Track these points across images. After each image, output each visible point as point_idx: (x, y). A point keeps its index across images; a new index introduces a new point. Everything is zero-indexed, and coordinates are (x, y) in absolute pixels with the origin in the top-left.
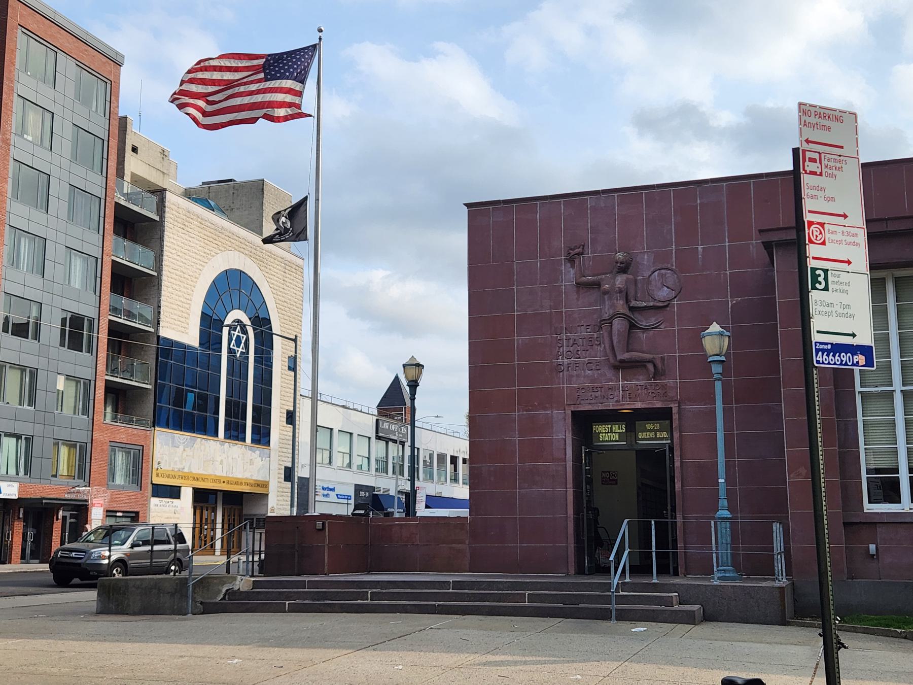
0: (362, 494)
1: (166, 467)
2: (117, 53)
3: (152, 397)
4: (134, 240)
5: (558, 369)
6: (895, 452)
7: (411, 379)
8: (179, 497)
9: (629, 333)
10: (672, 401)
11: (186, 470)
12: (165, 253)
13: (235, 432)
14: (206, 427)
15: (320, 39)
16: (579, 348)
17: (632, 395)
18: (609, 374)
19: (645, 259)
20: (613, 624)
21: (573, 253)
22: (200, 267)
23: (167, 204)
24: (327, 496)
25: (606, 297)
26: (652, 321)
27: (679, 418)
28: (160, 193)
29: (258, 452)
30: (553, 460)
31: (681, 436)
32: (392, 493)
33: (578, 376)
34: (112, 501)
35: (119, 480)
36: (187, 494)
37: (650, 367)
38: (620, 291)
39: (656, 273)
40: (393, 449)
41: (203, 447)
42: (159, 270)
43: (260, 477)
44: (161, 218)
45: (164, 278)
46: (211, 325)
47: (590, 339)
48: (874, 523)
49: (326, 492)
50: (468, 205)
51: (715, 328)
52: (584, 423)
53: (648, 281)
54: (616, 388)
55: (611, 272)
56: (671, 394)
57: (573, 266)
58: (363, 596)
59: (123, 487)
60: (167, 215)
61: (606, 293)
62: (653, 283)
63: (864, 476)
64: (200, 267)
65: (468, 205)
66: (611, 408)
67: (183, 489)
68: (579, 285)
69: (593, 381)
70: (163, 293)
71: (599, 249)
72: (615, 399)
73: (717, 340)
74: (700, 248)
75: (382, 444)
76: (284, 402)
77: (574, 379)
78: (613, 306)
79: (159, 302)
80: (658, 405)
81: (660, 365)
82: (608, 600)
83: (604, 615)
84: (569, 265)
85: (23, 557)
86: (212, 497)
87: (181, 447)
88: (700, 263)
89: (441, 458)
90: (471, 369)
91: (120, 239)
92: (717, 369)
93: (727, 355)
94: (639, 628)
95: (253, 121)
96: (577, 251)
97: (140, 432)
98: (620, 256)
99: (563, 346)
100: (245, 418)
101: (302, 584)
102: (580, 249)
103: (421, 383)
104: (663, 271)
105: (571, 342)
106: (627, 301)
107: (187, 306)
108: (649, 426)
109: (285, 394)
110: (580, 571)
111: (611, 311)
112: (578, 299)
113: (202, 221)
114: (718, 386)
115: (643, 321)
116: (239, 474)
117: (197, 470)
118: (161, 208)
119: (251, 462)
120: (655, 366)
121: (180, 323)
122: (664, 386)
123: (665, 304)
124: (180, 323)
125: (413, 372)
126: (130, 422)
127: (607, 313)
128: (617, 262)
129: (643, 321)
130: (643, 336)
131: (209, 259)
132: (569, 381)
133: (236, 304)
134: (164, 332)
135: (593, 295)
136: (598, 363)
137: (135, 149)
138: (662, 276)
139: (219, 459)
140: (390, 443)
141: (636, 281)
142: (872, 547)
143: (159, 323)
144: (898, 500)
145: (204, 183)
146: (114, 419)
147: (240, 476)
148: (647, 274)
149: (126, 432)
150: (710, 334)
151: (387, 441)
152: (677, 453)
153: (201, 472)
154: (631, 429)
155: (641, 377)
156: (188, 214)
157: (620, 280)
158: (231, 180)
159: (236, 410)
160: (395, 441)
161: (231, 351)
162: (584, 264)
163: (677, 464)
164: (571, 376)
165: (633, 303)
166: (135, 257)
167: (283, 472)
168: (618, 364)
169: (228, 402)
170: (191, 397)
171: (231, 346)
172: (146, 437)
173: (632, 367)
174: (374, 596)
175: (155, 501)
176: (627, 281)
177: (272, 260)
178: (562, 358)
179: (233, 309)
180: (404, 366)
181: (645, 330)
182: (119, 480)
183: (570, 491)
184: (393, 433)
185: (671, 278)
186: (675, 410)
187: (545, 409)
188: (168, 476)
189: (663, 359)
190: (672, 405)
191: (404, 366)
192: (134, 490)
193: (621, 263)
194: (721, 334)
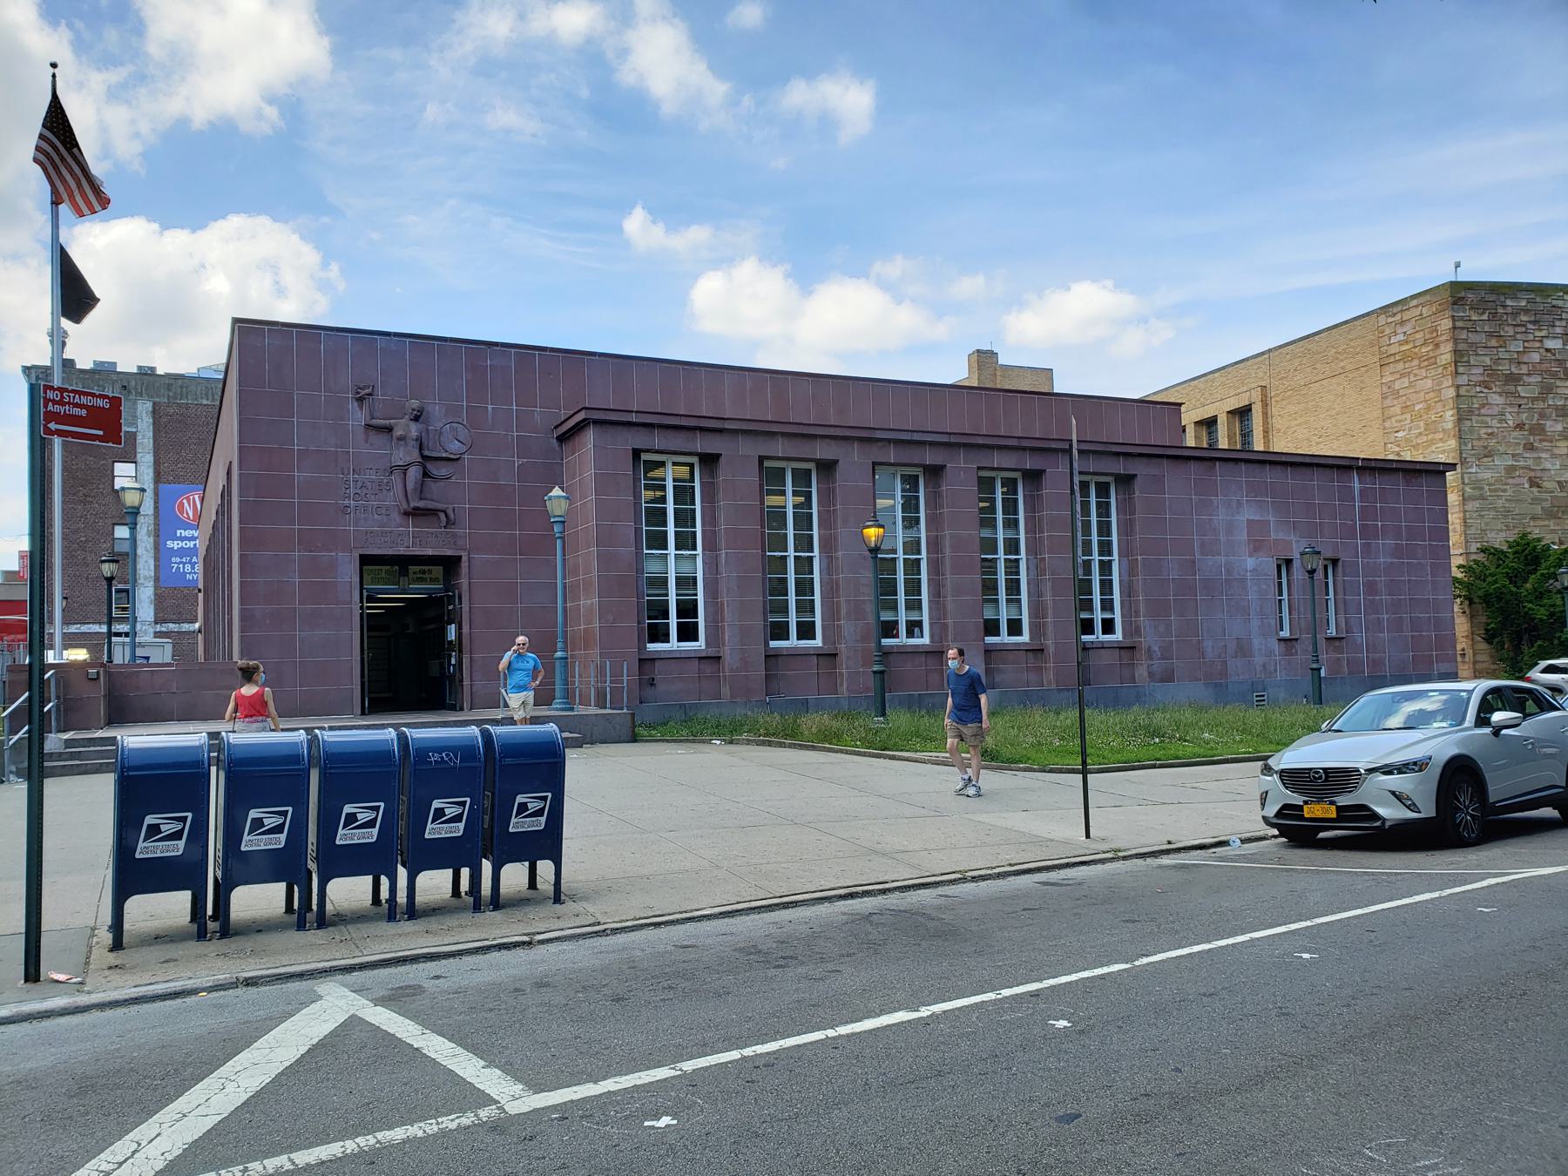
19: (436, 411)
37: (442, 516)
44: (59, 323)
56: (460, 543)
80: (449, 553)
81: (452, 516)
85: (363, 713)
106: (421, 449)
122: (454, 535)
135: (383, 437)
157: (414, 429)
165: (426, 453)
185: (463, 433)
186: (464, 559)
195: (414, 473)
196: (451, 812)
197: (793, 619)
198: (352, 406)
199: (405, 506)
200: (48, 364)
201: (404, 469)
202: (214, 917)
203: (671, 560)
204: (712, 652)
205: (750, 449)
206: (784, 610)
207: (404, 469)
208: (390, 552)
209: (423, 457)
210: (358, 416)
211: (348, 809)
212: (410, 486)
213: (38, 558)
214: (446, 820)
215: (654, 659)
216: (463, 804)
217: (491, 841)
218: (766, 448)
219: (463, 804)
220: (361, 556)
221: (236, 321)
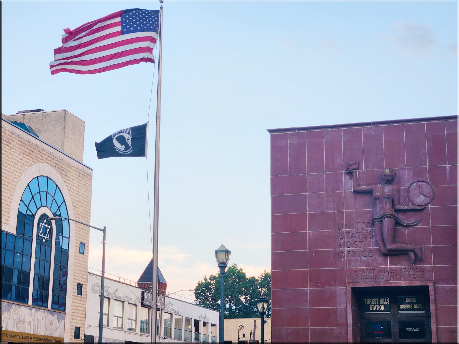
5: (340, 255)
7: (221, 261)
9: (395, 230)
10: (429, 281)
13: (40, 301)
15: (162, 7)
16: (356, 240)
17: (396, 274)
18: (380, 259)
19: (406, 174)
21: (351, 168)
22: (19, 175)
25: (377, 202)
26: (412, 220)
27: (435, 294)
29: (56, 316)
30: (338, 325)
31: (436, 309)
33: (355, 261)
38: (388, 198)
39: (415, 185)
41: (16, 311)
47: (365, 233)
50: (271, 131)
52: (360, 296)
53: (408, 190)
55: (380, 183)
57: (351, 178)
61: (376, 199)
62: (413, 192)
64: (19, 175)
65: (271, 131)
66: (382, 285)
69: (368, 264)
71: (371, 166)
72: (385, 279)
74: (448, 166)
75: (146, 310)
76: (76, 278)
77: (353, 263)
80: (418, 283)
84: (348, 177)
88: (448, 177)
89: (188, 321)
96: (354, 167)
98: (387, 171)
99: (344, 238)
102: (357, 166)
104: (420, 183)
105: (350, 234)
106: (393, 204)
107: (8, 203)
108: (408, 300)
109: (77, 271)
111: (382, 213)
112: (355, 203)
113: (21, 140)
119: (51, 323)
120: (415, 254)
122: (422, 270)
123: (422, 208)
125: (222, 257)
127: (378, 213)
128: (386, 176)
131: (26, 169)
132: (349, 265)
135: (366, 199)
138: (420, 187)
139: (28, 320)
141: (399, 191)
145: (20, 112)
151: (149, 307)
152: (433, 321)
153: (15, 330)
155: (404, 263)
156: (11, 135)
157: (387, 189)
158: (40, 110)
159: (43, 283)
162: (360, 178)
163: (434, 329)
165: (398, 207)
167: (74, 331)
168: (386, 252)
171: (40, 235)
177: (71, 170)
178: (344, 246)
179: (42, 206)
180: (216, 252)
181: (407, 226)
185: (426, 188)
186: (431, 288)
187: (330, 285)
189: (421, 249)
190: (429, 284)
191: (216, 252)
193: (389, 176)
195: (387, 222)
199: (383, 249)
200: (225, 319)
201: (381, 220)
207: (381, 220)
208: (374, 285)
210: (348, 185)
212: (385, 233)
213: (153, 258)
220: (353, 289)
221: (277, 135)
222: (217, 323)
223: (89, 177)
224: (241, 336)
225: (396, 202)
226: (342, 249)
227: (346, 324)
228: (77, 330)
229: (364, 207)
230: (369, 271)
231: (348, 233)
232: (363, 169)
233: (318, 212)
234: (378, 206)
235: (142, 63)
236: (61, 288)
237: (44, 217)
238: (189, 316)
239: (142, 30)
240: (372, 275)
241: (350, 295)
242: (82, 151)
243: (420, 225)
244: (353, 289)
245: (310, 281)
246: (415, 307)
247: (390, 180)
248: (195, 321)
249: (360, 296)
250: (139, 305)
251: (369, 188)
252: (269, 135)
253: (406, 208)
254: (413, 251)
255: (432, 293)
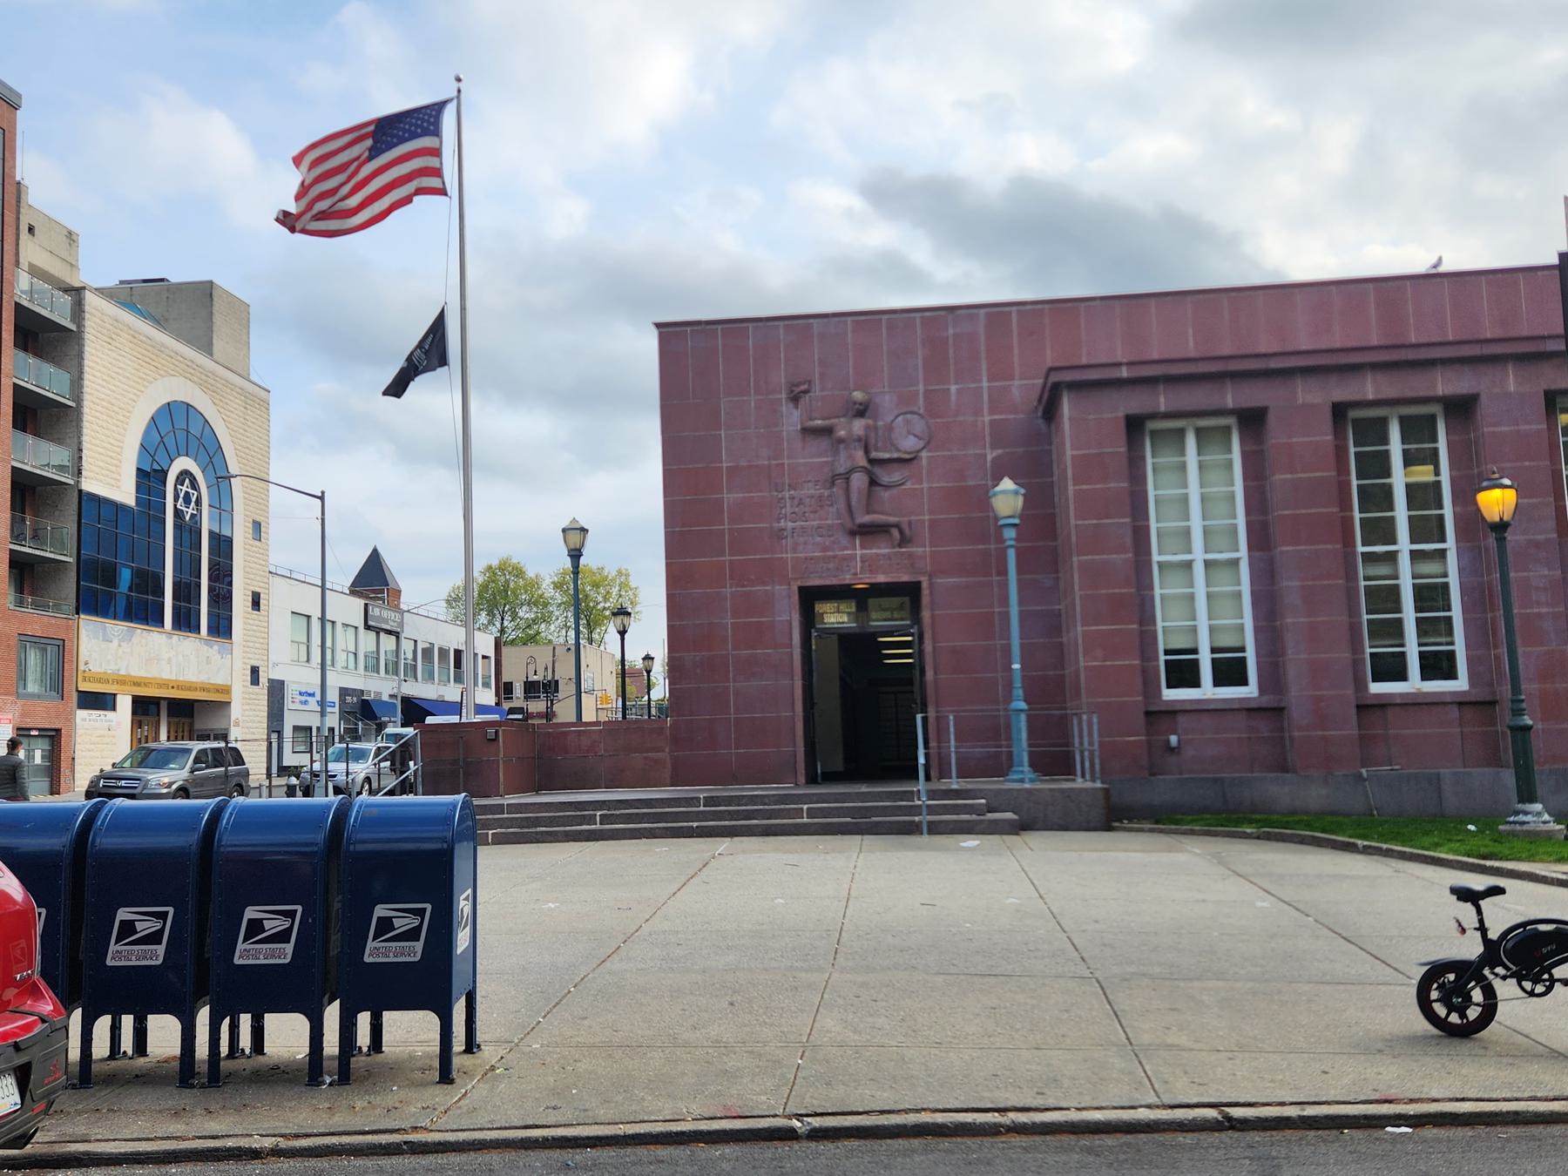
0: (349, 699)
1: (95, 668)
2: (11, 90)
3: (74, 574)
4: (39, 354)
5: (779, 535)
6: (1194, 630)
8: (114, 709)
9: (870, 494)
10: (923, 574)
11: (123, 672)
12: (86, 376)
13: (186, 621)
14: (152, 616)
17: (870, 564)
18: (844, 540)
19: (887, 402)
20: (925, 838)
21: (797, 390)
23: (87, 308)
24: (305, 703)
28: (77, 293)
31: (933, 617)
32: (385, 698)
34: (23, 715)
35: (32, 687)
36: (125, 704)
37: (895, 532)
38: (859, 440)
40: (388, 643)
42: (78, 399)
43: (219, 680)
45: (86, 410)
46: (150, 479)
47: (820, 497)
48: (1174, 712)
49: (304, 698)
50: (658, 325)
51: (1007, 484)
52: (810, 597)
53: (890, 428)
54: (853, 557)
58: (591, 820)
59: (39, 696)
60: (87, 323)
61: (841, 441)
63: (1162, 658)
65: (658, 325)
67: (119, 698)
68: (806, 431)
69: (825, 549)
70: (85, 431)
73: (1011, 498)
74: (953, 388)
75: (373, 635)
78: (851, 457)
79: (80, 443)
80: (905, 578)
81: (907, 531)
82: (916, 810)
83: (912, 829)
84: (791, 405)
86: (153, 708)
87: (116, 642)
89: (443, 653)
90: (667, 534)
91: (22, 354)
92: (1010, 534)
93: (1021, 517)
94: (971, 842)
95: (407, 200)
97: (59, 622)
98: (858, 395)
100: (175, 608)
101: (499, 809)
103: (585, 552)
106: (867, 452)
110: (812, 780)
111: (849, 465)
114: (1011, 554)
115: (885, 477)
116: (191, 676)
117: (138, 671)
118: (78, 310)
120: (901, 532)
121: (110, 474)
122: (910, 556)
124: (110, 474)
125: (575, 539)
126: (45, 607)
129: (885, 477)
130: (886, 495)
132: (794, 550)
133: (183, 450)
134: (89, 485)
135: (824, 443)
136: (830, 527)
137: (31, 230)
138: (907, 422)
140: (382, 634)
141: (876, 428)
142: (1174, 739)
143: (80, 472)
144: (1195, 683)
146: (20, 603)
147: (194, 679)
148: (889, 418)
149: (37, 621)
150: (1003, 492)
151: (378, 631)
153: (143, 674)
154: (862, 607)
157: (858, 426)
159: (187, 592)
160: (389, 632)
161: (178, 514)
164: (796, 544)
165: (874, 455)
166: (44, 379)
169: (176, 585)
170: (125, 576)
172: (68, 628)
173: (872, 533)
174: (604, 819)
175: (82, 715)
176: (867, 427)
180: (564, 530)
181: (887, 487)
182: (32, 687)
183: (798, 683)
184: (386, 621)
185: (919, 425)
186: (925, 585)
187: (764, 583)
188: (100, 681)
189: (910, 523)
191: (564, 530)
192: (54, 703)
194: (1016, 493)
195: (859, 481)
196: (273, 925)
197: (1412, 649)
198: (786, 407)
199: (849, 525)
202: (1229, 1118)
203: (1404, 562)
204: (1267, 701)
205: (1316, 396)
206: (1396, 629)
207: (846, 477)
208: (834, 582)
209: (872, 461)
211: (123, 914)
214: (266, 940)
215: (1175, 712)
216: (291, 915)
217: (328, 974)
218: (1343, 391)
219: (291, 915)
220: (800, 588)
222: (492, 654)
223: (265, 404)
224: (531, 673)
225: (871, 447)
226: (782, 524)
227: (790, 646)
228: (255, 671)
229: (819, 456)
230: (826, 559)
231: (792, 498)
232: (817, 392)
233: (743, 463)
234: (843, 455)
235: (416, 199)
236: (221, 599)
237: (185, 475)
238: (445, 645)
239: (403, 141)
240: (831, 566)
241: (796, 598)
242: (248, 356)
243: (908, 485)
244: (800, 588)
245: (731, 578)
246: (896, 615)
247: (862, 411)
248: (440, 649)
249: (810, 597)
250: (361, 625)
251: (827, 422)
252: (655, 333)
253: (887, 456)
254: (897, 526)
255: (925, 592)
